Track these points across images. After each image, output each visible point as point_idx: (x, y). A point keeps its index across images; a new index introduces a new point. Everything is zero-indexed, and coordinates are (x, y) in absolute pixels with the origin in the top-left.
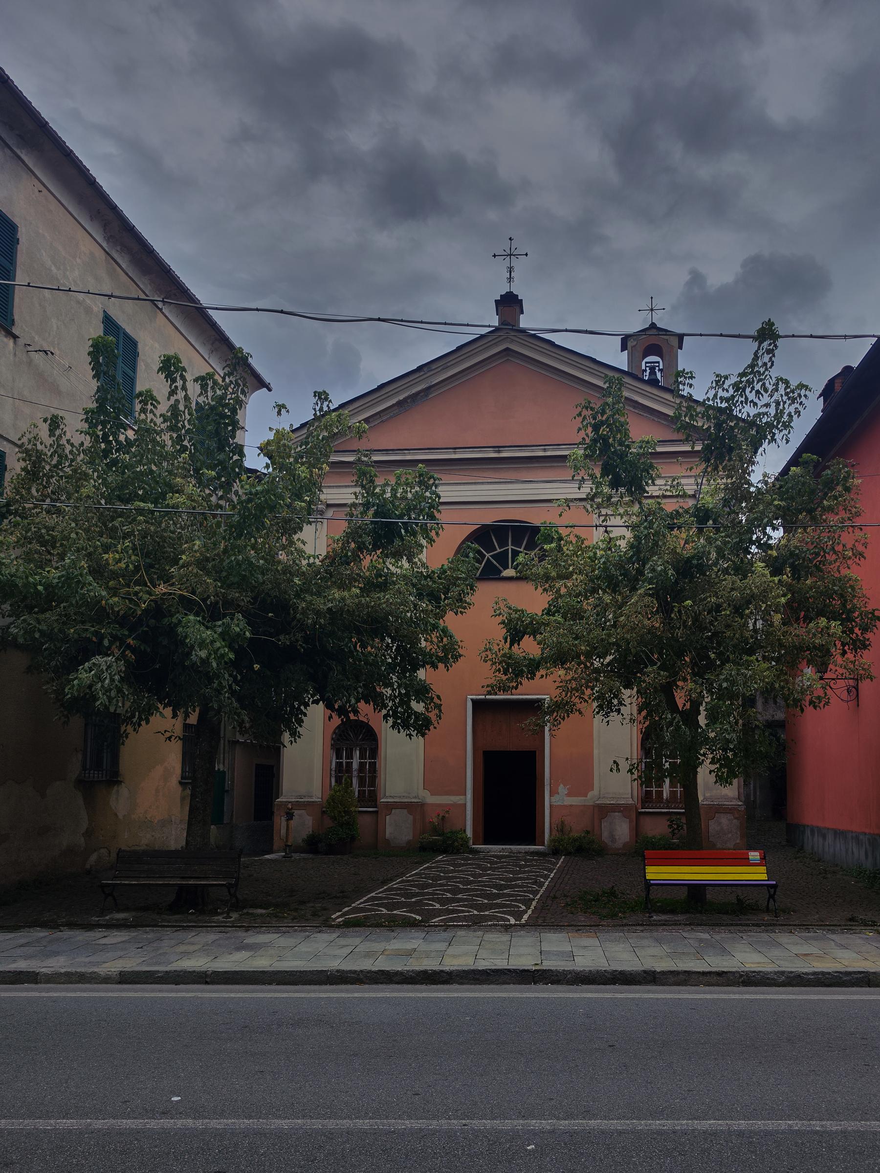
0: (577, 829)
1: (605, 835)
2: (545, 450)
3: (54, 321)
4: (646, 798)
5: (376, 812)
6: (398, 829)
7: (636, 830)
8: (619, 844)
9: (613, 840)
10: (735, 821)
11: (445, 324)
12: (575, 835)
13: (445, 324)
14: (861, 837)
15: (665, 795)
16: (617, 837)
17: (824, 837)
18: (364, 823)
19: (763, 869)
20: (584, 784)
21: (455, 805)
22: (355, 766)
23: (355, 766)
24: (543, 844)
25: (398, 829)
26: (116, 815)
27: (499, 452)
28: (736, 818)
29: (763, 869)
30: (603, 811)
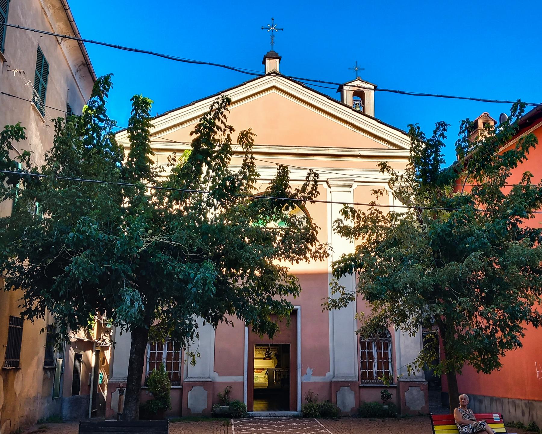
0: (321, 398)
1: (339, 403)
2: (298, 150)
3: (19, 51)
4: (363, 376)
5: (181, 389)
6: (197, 400)
7: (358, 398)
8: (348, 409)
9: (344, 406)
10: (421, 392)
11: (320, 82)
12: (320, 403)
13: (320, 82)
14: (517, 402)
15: (374, 374)
16: (347, 404)
17: (481, 402)
18: (173, 396)
19: (502, 425)
20: (322, 366)
21: (235, 383)
22: (164, 355)
23: (164, 355)
24: (296, 411)
25: (197, 400)
26: (16, 394)
27: (269, 149)
28: (422, 390)
29: (502, 425)
30: (335, 386)
